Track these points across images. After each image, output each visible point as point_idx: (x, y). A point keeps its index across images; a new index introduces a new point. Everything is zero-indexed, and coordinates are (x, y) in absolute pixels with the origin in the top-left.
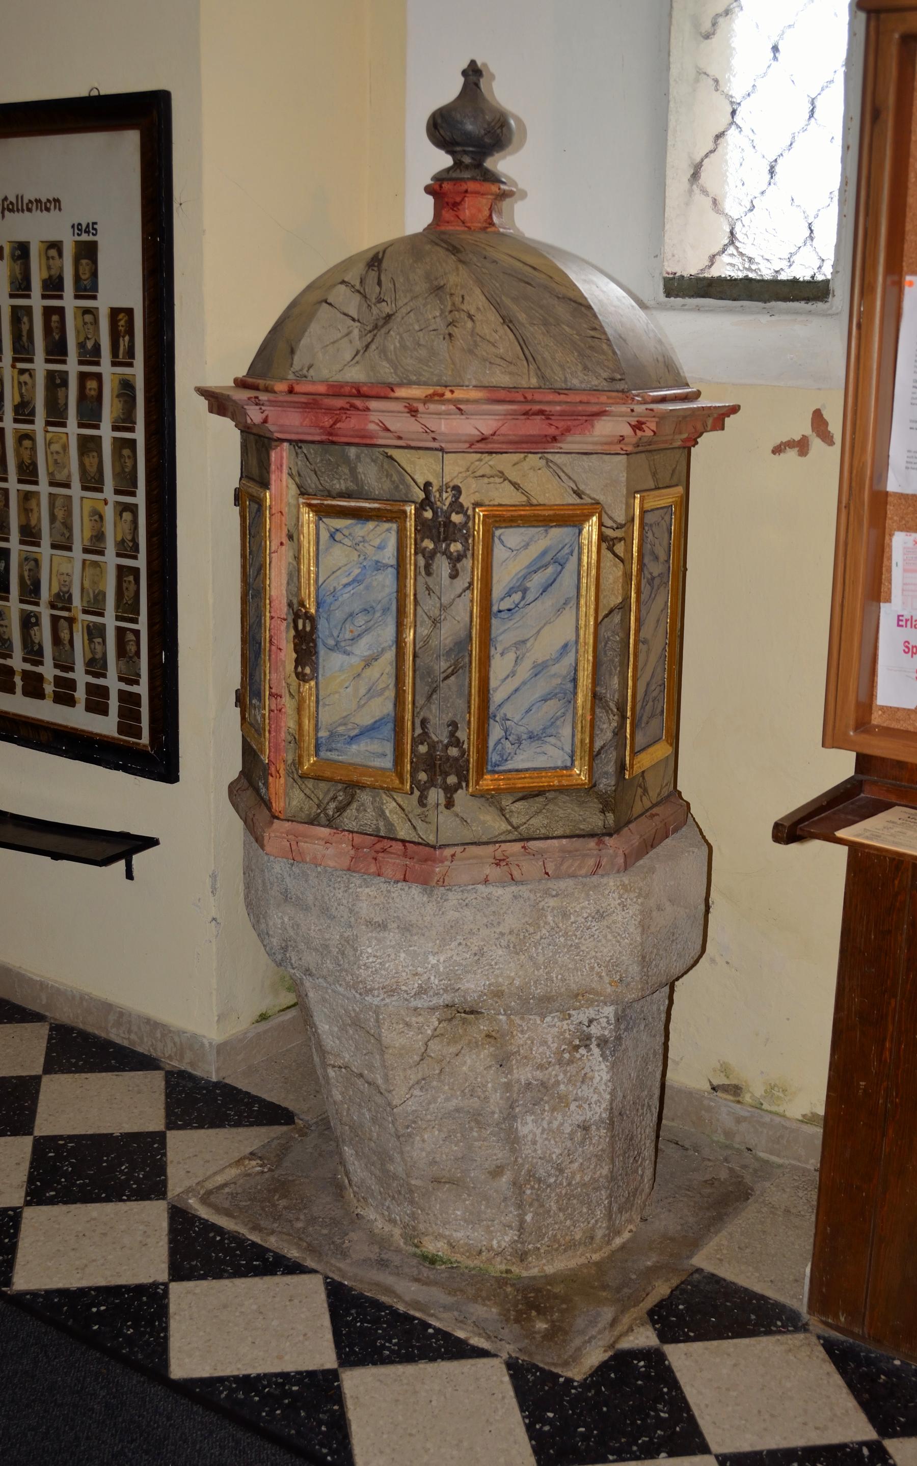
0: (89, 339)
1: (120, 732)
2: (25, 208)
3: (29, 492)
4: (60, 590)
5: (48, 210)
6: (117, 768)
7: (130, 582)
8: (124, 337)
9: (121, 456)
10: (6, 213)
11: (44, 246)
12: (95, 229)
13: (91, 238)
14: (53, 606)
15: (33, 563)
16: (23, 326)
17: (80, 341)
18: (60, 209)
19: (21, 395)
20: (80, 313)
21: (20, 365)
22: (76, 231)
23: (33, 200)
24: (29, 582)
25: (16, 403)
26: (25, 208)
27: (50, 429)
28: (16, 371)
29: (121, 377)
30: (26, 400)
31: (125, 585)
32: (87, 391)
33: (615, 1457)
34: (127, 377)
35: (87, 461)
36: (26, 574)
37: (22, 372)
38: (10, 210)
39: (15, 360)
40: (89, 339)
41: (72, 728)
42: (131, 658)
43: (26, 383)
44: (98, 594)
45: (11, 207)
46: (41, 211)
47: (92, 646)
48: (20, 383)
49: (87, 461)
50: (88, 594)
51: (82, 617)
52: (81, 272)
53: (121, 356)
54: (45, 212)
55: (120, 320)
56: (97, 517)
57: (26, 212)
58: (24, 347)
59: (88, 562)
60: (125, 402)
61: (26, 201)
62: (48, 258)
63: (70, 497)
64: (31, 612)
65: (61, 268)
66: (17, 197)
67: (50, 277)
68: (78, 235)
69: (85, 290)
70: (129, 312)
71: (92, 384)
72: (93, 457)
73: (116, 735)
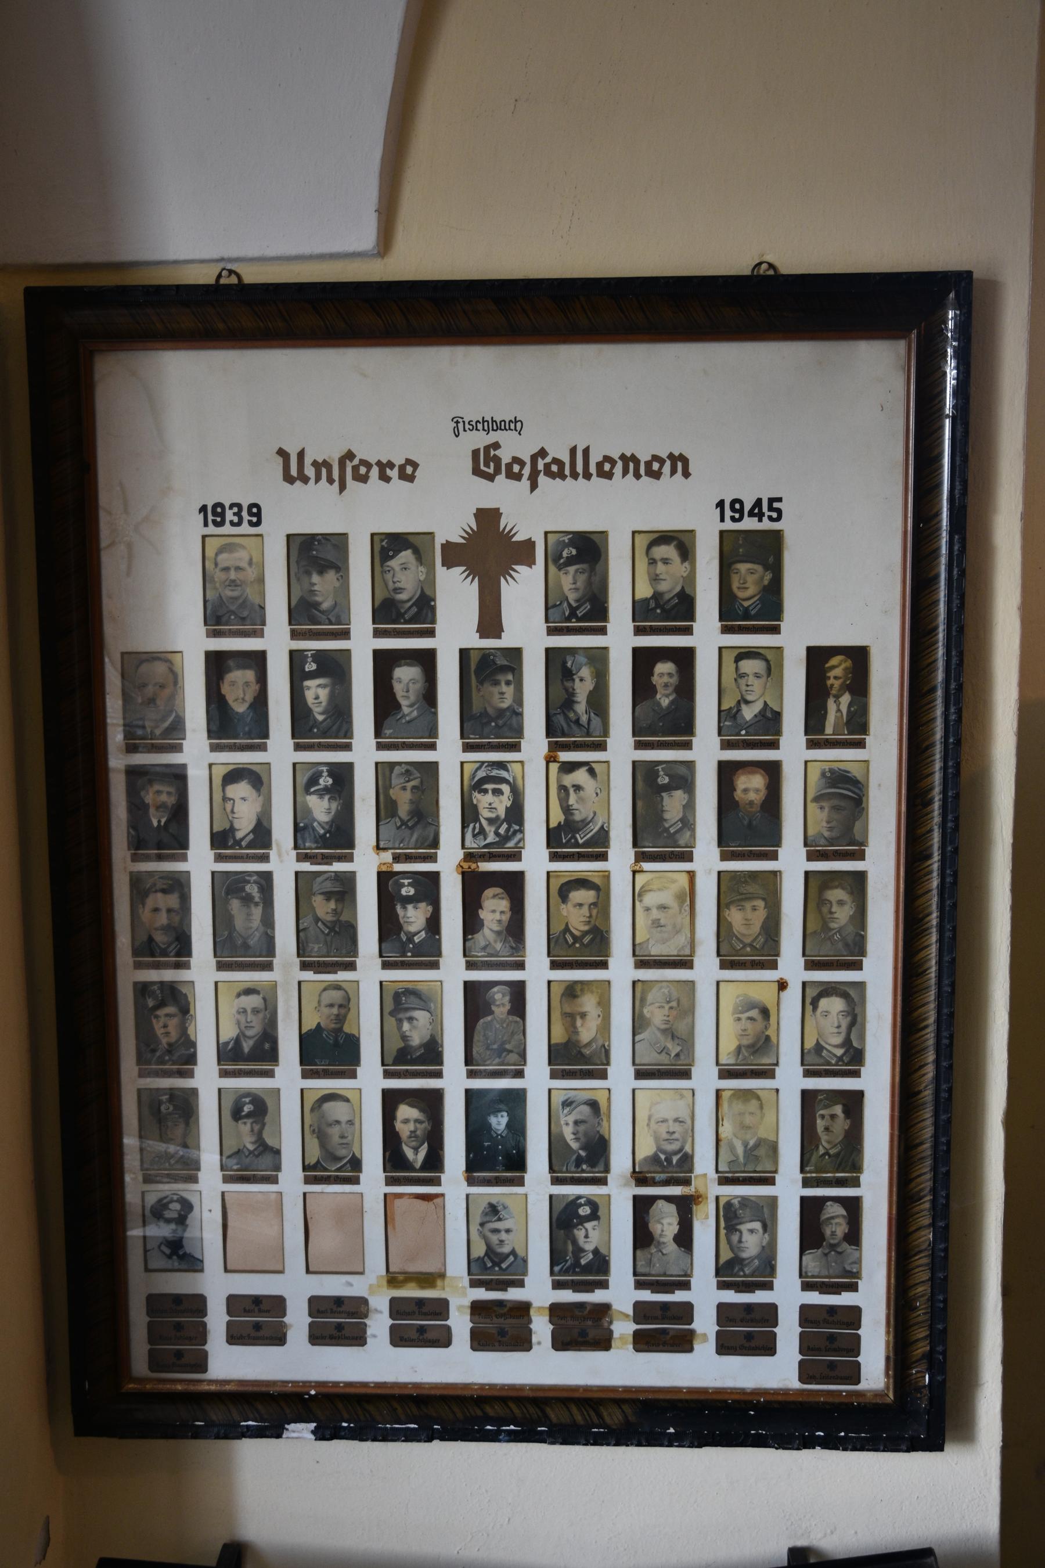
0: (747, 702)
1: (801, 1380)
2: (593, 469)
3: (576, 982)
4: (657, 1139)
5: (656, 475)
6: (808, 1443)
7: (833, 1117)
8: (837, 697)
9: (822, 902)
10: (542, 479)
11: (642, 542)
12: (779, 511)
13: (766, 525)
14: (640, 1179)
15: (586, 1110)
16: (577, 684)
17: (725, 706)
18: (686, 474)
19: (567, 810)
20: (729, 658)
21: (565, 756)
22: (728, 513)
23: (616, 456)
24: (574, 1145)
25: (553, 824)
26: (593, 469)
27: (647, 866)
28: (554, 767)
29: (826, 766)
30: (578, 817)
31: (820, 1124)
32: (738, 795)
33: (162, 824)
34: (842, 766)
35: (735, 916)
36: (568, 1133)
37: (570, 767)
38: (548, 473)
39: (555, 747)
40: (747, 702)
41: (691, 1390)
42: (833, 1247)
43: (578, 788)
44: (757, 1145)
45: (554, 468)
46: (637, 476)
47: (735, 1238)
48: (563, 788)
49: (735, 916)
50: (732, 1148)
51: (716, 1190)
52: (735, 585)
53: (829, 729)
54: (645, 479)
55: (834, 667)
56: (754, 1013)
57: (569, 479)
58: (577, 722)
59: (725, 1095)
60: (835, 808)
61: (595, 458)
62: (653, 562)
63: (692, 983)
64: (579, 1197)
65: (691, 579)
66: (573, 451)
67: (657, 596)
68: (733, 519)
69: (746, 616)
70: (859, 657)
71: (406, 676)
72: (754, 909)
73: (795, 1384)
